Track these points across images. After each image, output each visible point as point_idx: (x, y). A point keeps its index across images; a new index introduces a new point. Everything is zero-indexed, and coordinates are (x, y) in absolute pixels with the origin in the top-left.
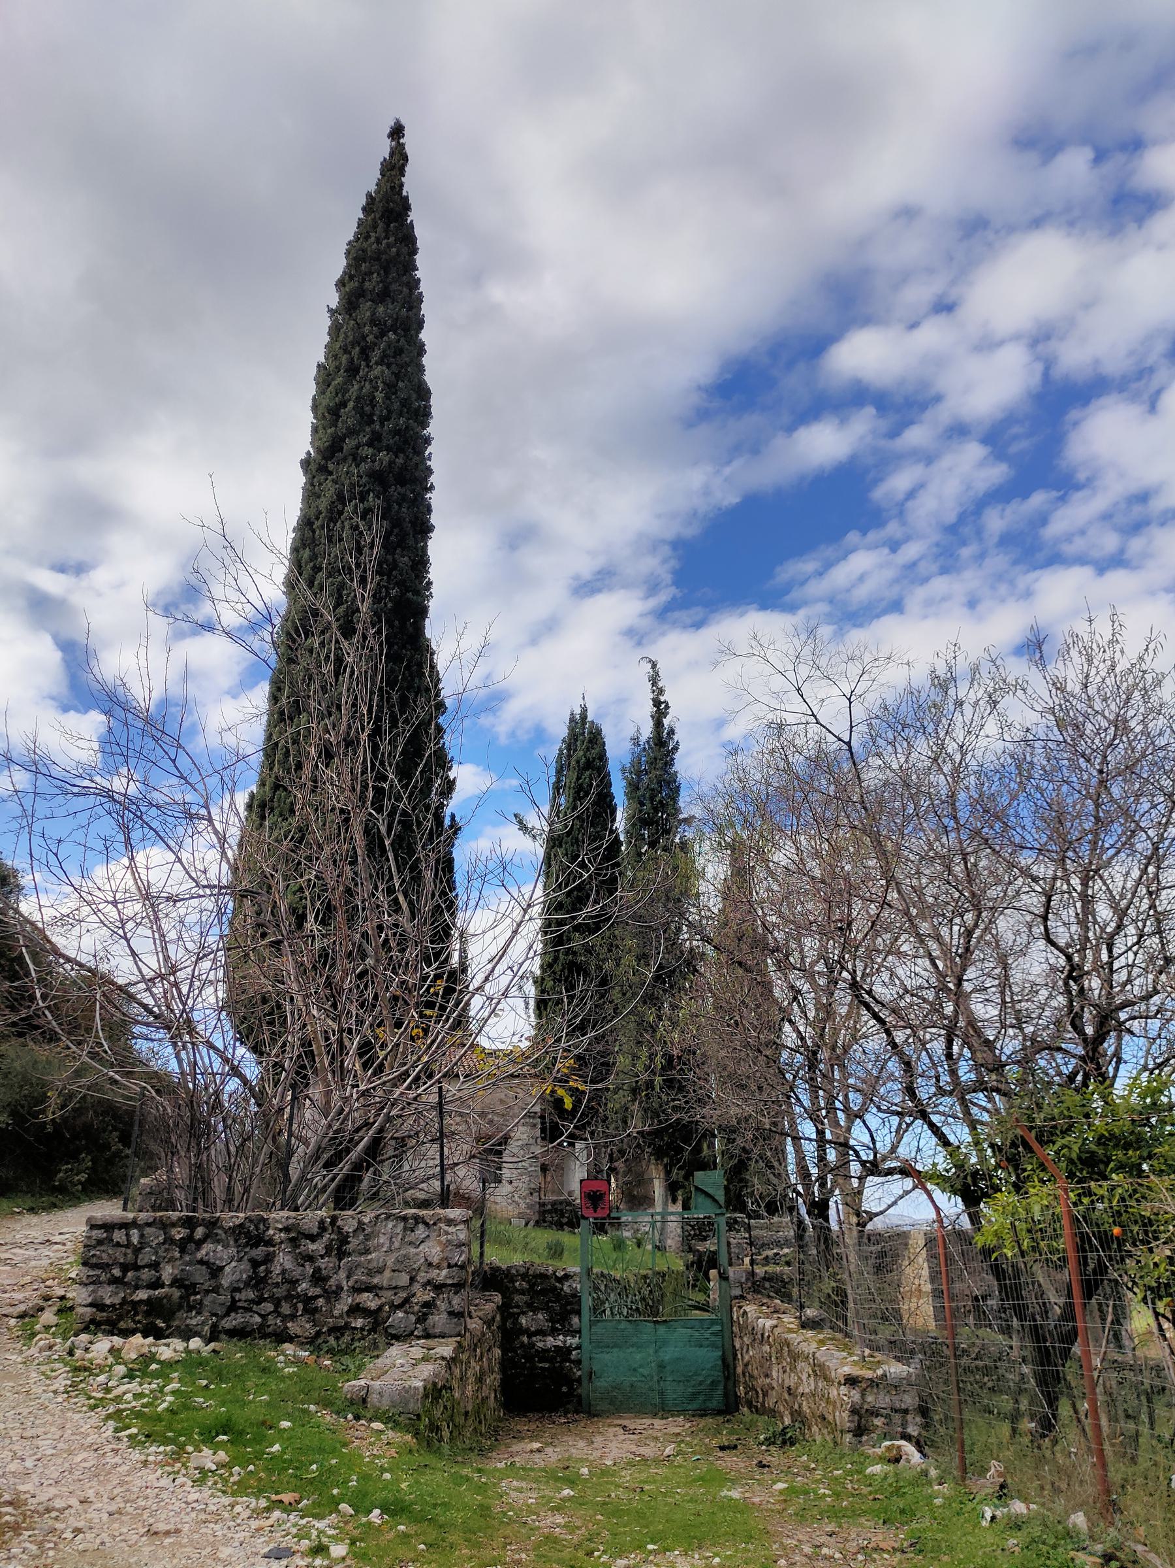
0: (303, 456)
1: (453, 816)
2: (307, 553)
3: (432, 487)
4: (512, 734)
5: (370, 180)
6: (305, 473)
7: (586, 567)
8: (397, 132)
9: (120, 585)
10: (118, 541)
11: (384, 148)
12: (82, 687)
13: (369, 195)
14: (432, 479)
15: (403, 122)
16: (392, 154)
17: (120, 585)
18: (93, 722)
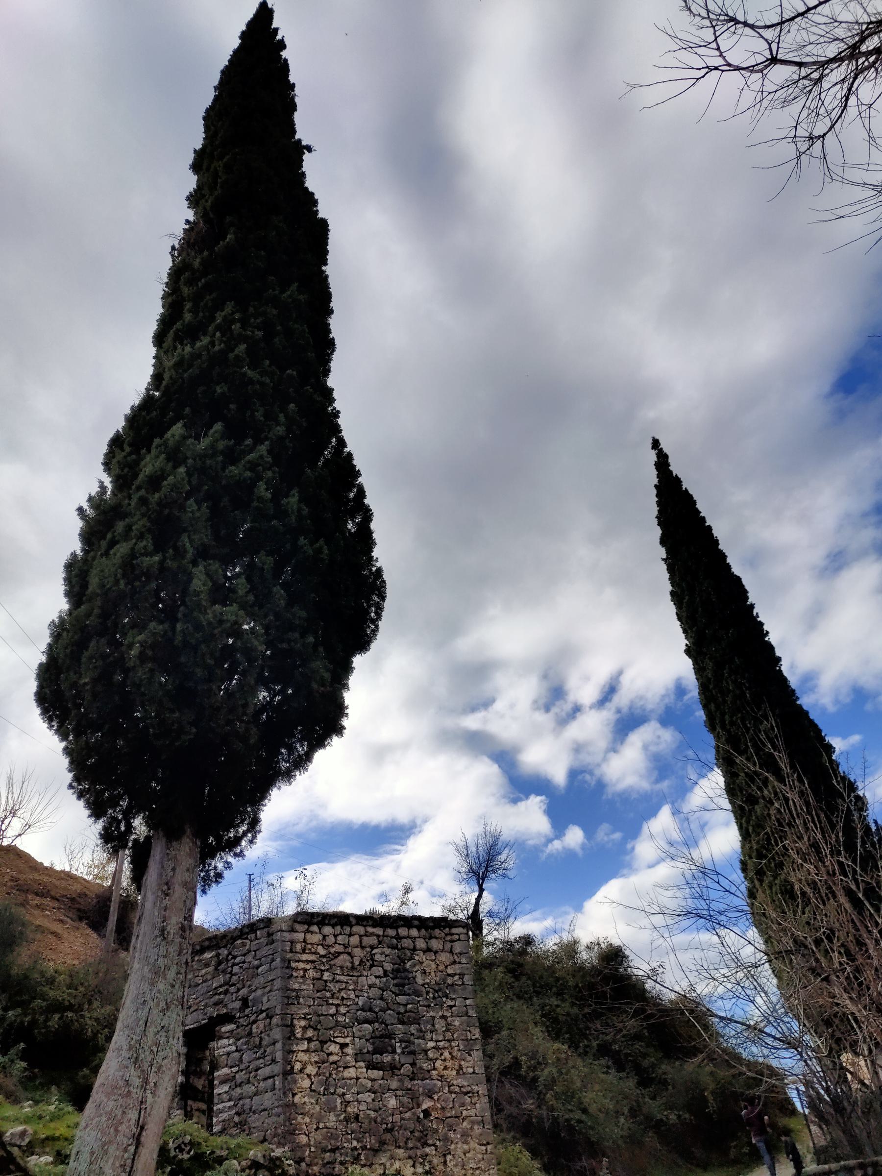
0: (684, 648)
1: (876, 822)
2: (712, 707)
3: (767, 632)
4: (837, 701)
5: (652, 477)
6: (690, 657)
7: (817, 556)
8: (656, 444)
9: (512, 706)
10: (500, 679)
11: (653, 456)
12: (521, 785)
13: (656, 486)
14: (766, 628)
15: (657, 437)
16: (658, 457)
17: (512, 706)
18: (535, 805)
